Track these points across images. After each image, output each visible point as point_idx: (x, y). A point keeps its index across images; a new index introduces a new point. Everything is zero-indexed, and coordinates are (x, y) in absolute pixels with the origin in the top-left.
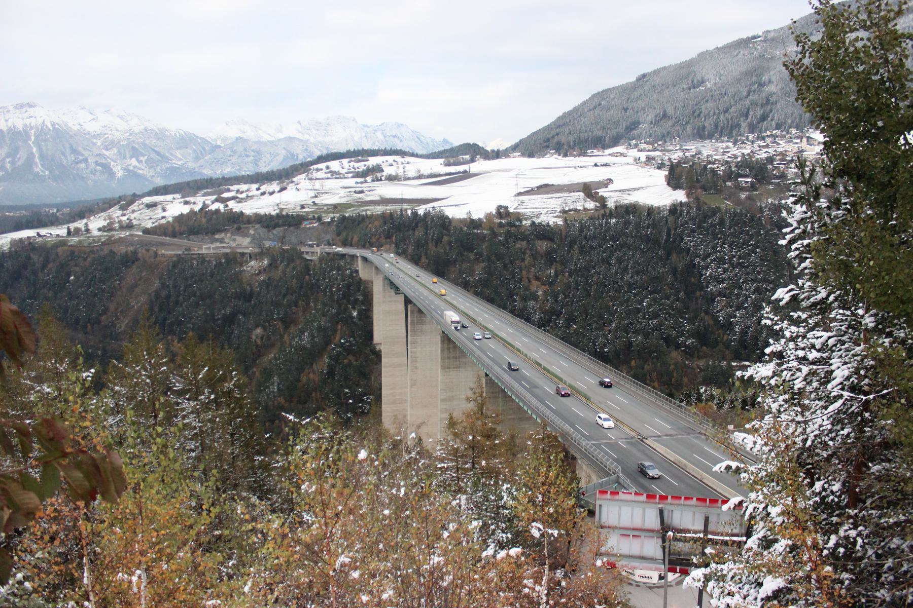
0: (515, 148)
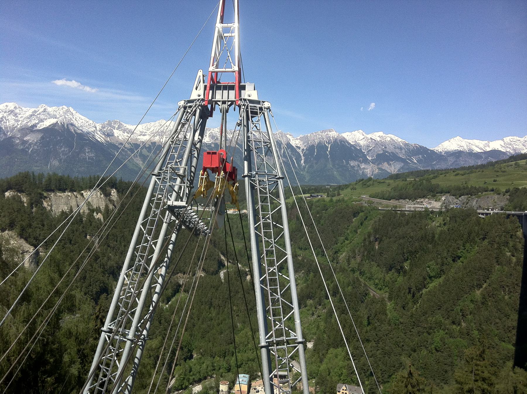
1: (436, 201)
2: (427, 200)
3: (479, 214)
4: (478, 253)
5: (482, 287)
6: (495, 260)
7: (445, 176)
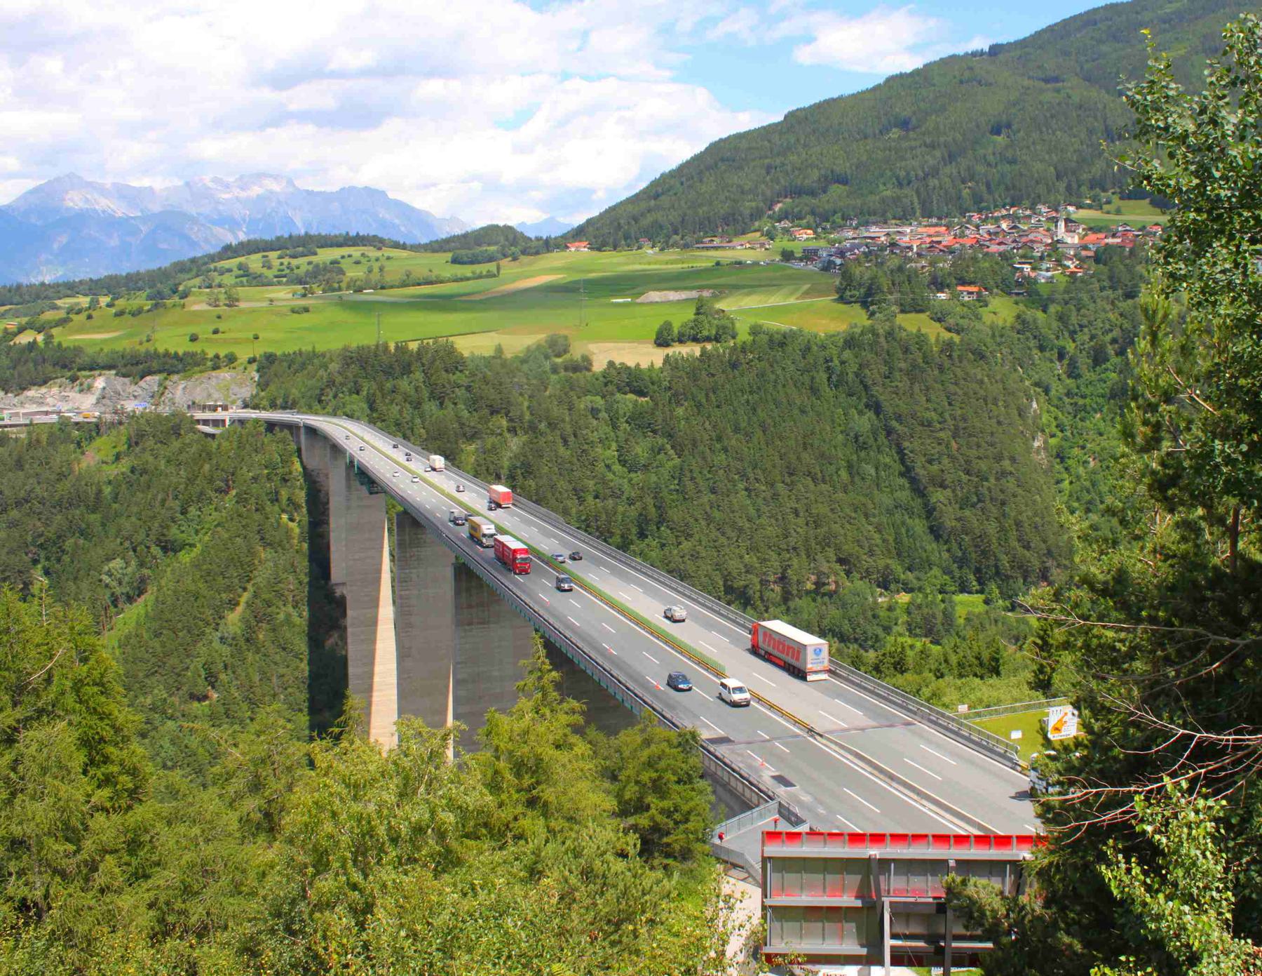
0: (579, 233)
1: (81, 391)
2: (55, 390)
3: (198, 421)
4: (218, 525)
5: (237, 604)
6: (258, 537)
7: (90, 317)
